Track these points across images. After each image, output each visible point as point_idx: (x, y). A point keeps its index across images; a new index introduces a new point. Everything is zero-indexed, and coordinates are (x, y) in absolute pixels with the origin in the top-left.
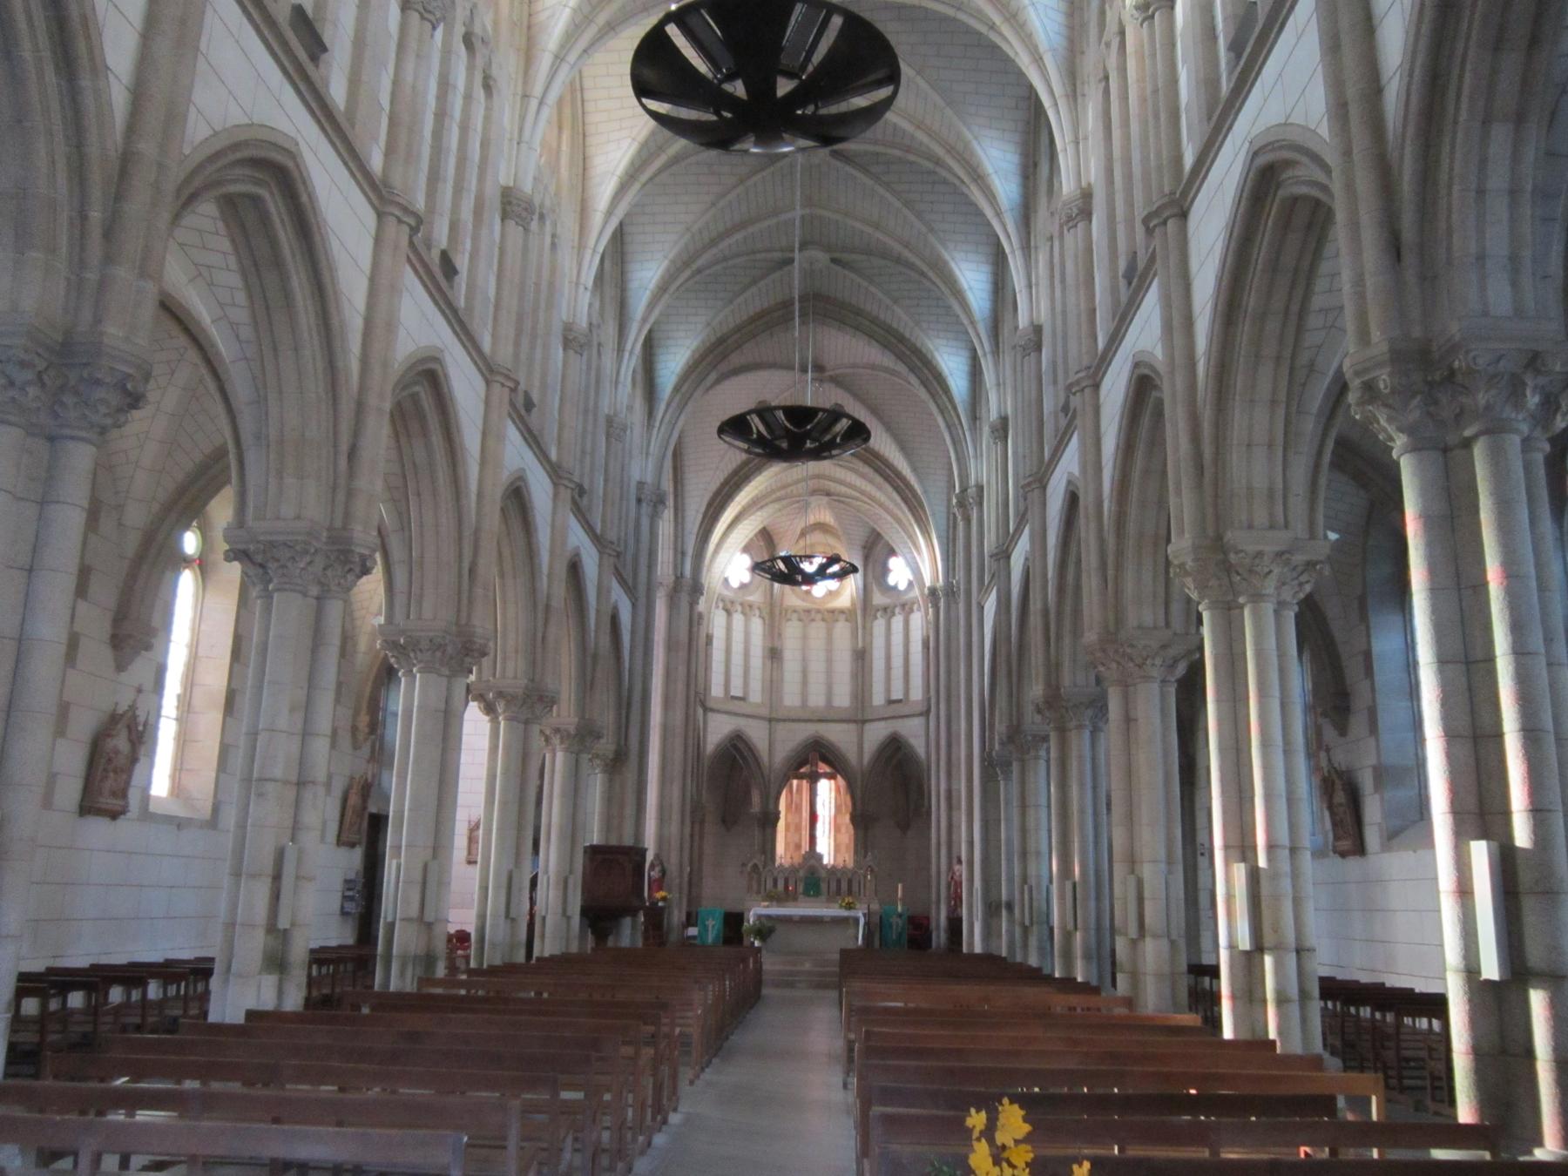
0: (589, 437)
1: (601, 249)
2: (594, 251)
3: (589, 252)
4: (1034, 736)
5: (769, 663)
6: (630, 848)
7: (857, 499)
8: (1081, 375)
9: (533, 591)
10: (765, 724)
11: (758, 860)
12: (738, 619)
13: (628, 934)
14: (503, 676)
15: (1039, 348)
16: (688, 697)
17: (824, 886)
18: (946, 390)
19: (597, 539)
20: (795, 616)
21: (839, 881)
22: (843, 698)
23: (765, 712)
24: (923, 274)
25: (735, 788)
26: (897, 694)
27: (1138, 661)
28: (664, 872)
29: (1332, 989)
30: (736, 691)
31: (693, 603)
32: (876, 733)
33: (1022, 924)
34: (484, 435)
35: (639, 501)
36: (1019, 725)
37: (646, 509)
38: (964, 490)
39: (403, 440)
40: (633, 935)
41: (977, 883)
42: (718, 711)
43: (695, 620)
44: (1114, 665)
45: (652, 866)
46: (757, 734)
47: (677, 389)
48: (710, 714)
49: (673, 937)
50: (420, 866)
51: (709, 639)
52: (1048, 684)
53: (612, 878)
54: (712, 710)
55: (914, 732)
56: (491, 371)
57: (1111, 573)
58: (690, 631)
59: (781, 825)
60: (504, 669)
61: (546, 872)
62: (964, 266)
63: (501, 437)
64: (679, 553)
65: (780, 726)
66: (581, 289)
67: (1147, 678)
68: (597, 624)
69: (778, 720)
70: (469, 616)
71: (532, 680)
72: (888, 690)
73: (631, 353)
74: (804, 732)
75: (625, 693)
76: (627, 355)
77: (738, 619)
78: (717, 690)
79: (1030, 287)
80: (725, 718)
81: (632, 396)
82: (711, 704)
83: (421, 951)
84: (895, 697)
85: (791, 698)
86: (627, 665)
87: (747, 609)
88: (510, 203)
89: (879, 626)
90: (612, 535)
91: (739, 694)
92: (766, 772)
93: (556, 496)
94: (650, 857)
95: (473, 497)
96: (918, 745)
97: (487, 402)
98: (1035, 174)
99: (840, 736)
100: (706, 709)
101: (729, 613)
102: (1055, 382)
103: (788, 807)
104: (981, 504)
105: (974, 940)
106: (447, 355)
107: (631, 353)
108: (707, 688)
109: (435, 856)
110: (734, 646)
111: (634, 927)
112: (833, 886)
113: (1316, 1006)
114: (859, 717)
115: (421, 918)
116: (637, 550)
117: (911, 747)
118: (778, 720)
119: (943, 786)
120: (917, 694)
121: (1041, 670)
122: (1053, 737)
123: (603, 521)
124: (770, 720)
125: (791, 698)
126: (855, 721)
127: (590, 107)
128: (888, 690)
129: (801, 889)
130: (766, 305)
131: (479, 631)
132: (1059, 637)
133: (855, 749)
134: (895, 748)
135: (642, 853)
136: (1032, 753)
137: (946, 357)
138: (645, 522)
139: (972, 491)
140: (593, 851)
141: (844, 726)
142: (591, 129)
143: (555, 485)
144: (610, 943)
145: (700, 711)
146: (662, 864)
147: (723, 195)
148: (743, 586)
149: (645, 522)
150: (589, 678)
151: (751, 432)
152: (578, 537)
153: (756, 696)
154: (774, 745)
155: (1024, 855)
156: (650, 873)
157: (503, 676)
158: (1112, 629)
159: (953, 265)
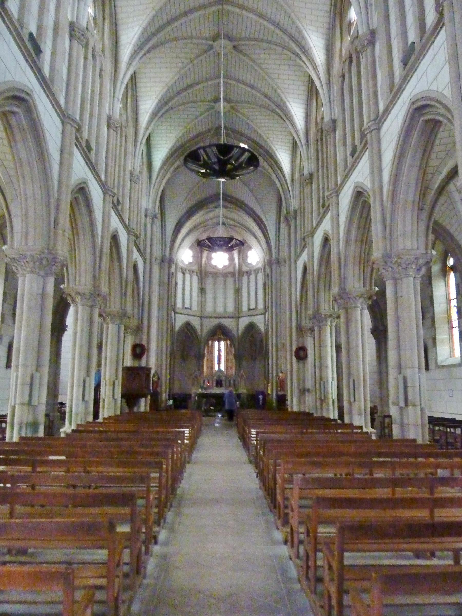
0: (122, 168)
1: (125, 82)
2: (122, 82)
3: (119, 83)
4: (325, 315)
5: (200, 294)
6: (144, 368)
7: (236, 226)
8: (370, 123)
9: (94, 247)
10: (199, 318)
11: (197, 373)
12: (188, 276)
13: (143, 405)
14: (80, 284)
15: (334, 130)
16: (168, 307)
17: (223, 383)
18: (281, 169)
19: (126, 227)
20: (210, 276)
21: (230, 381)
22: (231, 309)
23: (199, 314)
24: (297, 55)
25: (188, 345)
26: (253, 306)
27: (404, 266)
28: (159, 378)
29: (433, 421)
30: (187, 305)
31: (169, 267)
32: (244, 322)
33: (320, 399)
34: (62, 151)
35: (146, 216)
36: (318, 310)
37: (149, 220)
38: (288, 213)
39: (13, 143)
40: (145, 406)
41: (295, 381)
42: (180, 314)
43: (171, 276)
44: (390, 269)
45: (154, 376)
46: (196, 323)
47: (162, 167)
48: (177, 315)
49: (163, 405)
50: (29, 376)
51: (176, 284)
52: (341, 288)
53: (136, 383)
54: (178, 313)
55: (260, 322)
56: (64, 115)
57: (388, 222)
58: (169, 279)
59: (205, 359)
60: (80, 280)
61: (105, 379)
62: (292, 104)
63: (71, 154)
64: (163, 244)
65: (205, 320)
66: (116, 99)
67: (408, 276)
68: (127, 267)
69: (204, 317)
70: (55, 244)
71: (95, 287)
72: (249, 305)
73: (141, 143)
74: (216, 322)
75: (141, 301)
76: (139, 144)
77: (188, 276)
78: (179, 305)
79: (330, 102)
80: (181, 316)
81: (141, 169)
82: (177, 310)
83: (30, 420)
84: (251, 307)
85: (209, 308)
86: (142, 289)
87: (191, 272)
88: (74, 30)
89: (245, 279)
90: (133, 226)
91: (188, 306)
92: (199, 337)
93: (104, 200)
94: (153, 372)
95: (56, 183)
96: (262, 327)
97: (63, 133)
98: (332, 49)
99: (229, 323)
100: (175, 313)
101: (184, 274)
102: (345, 144)
103: (208, 352)
104: (296, 219)
105: (294, 405)
106: (34, 93)
107: (141, 143)
108: (175, 305)
109: (37, 370)
110: (186, 291)
111: (146, 402)
112: (228, 384)
113: (427, 426)
114: (237, 316)
115: (29, 403)
116: (146, 238)
117: (258, 326)
118: (204, 317)
119: (274, 342)
120: (261, 306)
121: (337, 281)
122: (342, 313)
123: (129, 220)
124: (201, 317)
125: (209, 308)
126: (235, 318)
127: (119, 10)
128: (249, 305)
129: (215, 384)
130: (201, 131)
131: (60, 252)
132: (346, 265)
133: (236, 329)
134: (251, 327)
135: (149, 369)
136: (324, 323)
137: (280, 153)
138: (149, 226)
139: (292, 213)
140: (127, 370)
141: (232, 320)
142: (119, 22)
143: (104, 194)
144: (135, 409)
145: (173, 313)
146: (158, 375)
147: (184, 67)
148: (190, 263)
149: (149, 226)
150: (124, 291)
151: (200, 161)
152: (115, 223)
153: (195, 307)
154: (202, 327)
155: (321, 367)
156: (153, 378)
157: (80, 284)
158: (388, 251)
159: (288, 103)
